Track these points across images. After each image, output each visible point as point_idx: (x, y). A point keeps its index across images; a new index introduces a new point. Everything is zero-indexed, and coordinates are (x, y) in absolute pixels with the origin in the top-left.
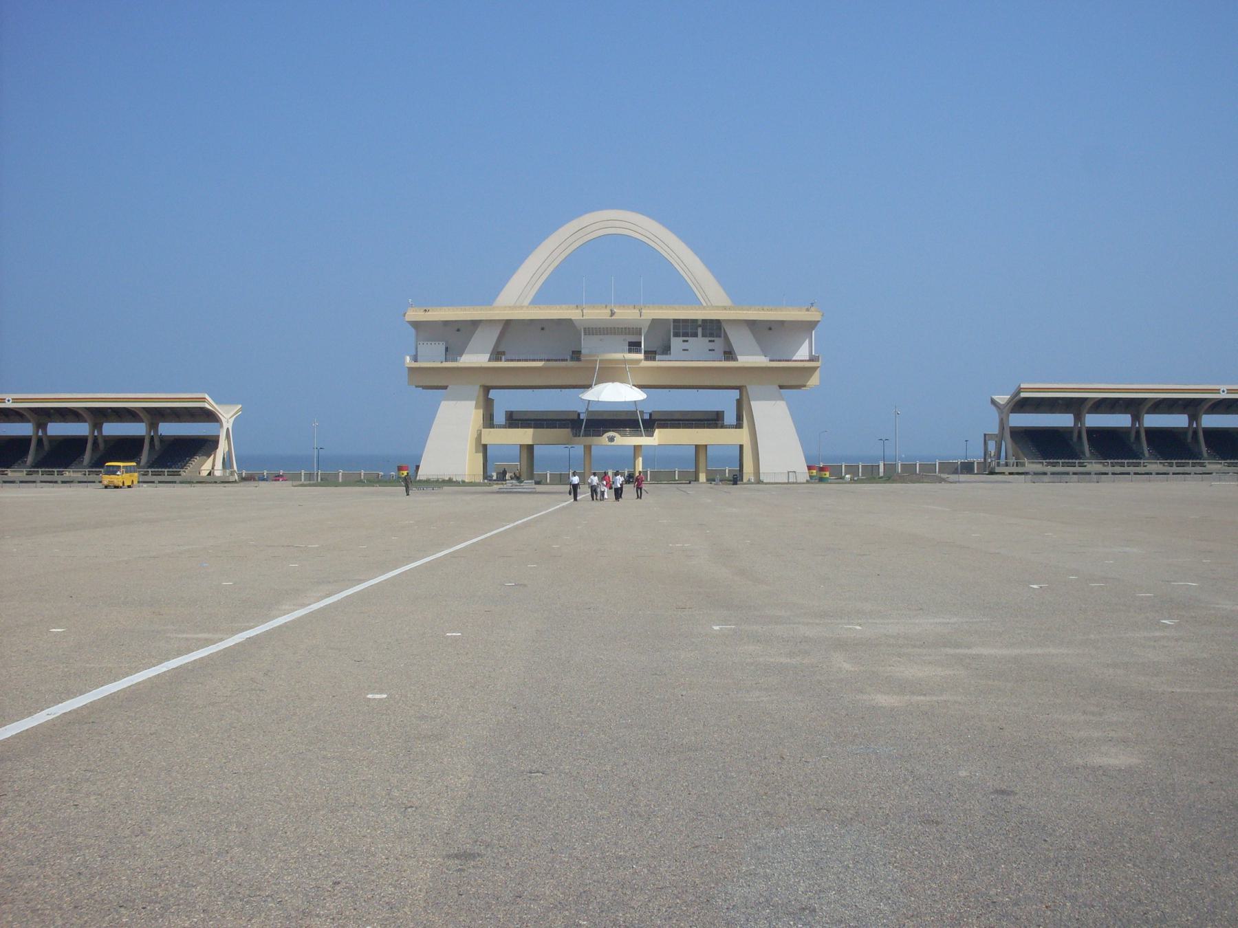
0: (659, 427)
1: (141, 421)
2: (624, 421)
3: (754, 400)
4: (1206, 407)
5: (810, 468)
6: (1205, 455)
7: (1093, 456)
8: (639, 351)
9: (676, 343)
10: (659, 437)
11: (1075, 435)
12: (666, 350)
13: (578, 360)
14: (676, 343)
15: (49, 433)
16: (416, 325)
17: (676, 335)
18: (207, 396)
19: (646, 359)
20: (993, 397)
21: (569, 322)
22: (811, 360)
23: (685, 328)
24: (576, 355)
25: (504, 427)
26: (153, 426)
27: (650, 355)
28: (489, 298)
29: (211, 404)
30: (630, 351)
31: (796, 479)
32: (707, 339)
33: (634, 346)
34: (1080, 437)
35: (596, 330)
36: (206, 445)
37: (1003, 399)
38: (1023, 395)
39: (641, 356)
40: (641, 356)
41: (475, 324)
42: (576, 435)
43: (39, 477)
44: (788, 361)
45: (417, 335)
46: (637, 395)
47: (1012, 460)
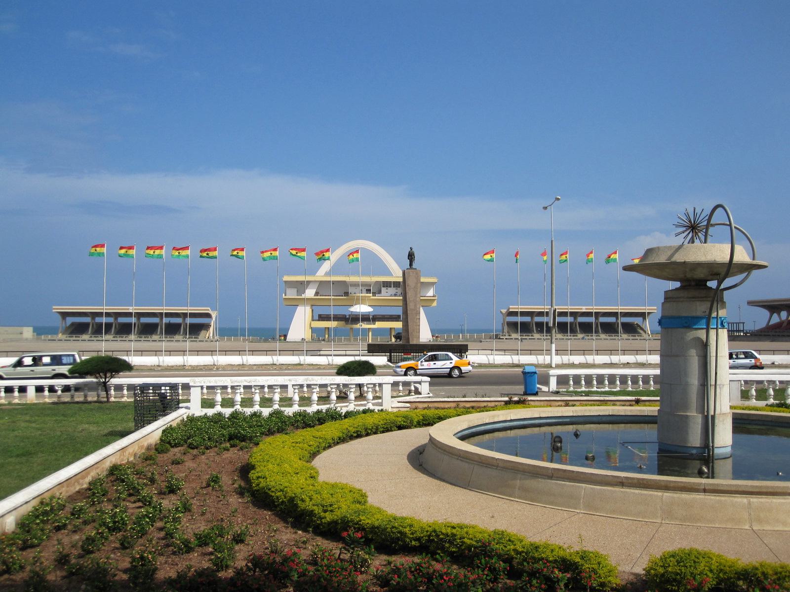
0: (378, 321)
1: (181, 317)
2: (366, 318)
3: (737, 244)
4: (579, 314)
5: (433, 336)
6: (600, 332)
7: (581, 333)
8: (370, 293)
9: (384, 290)
10: (379, 325)
11: (574, 324)
12: (380, 292)
13: (348, 296)
14: (384, 290)
15: (96, 321)
16: (286, 282)
17: (383, 287)
18: (209, 308)
19: (373, 296)
20: (502, 310)
21: (345, 282)
22: (433, 296)
23: (387, 284)
24: (346, 294)
25: (319, 320)
26: (116, 319)
27: (374, 294)
28: (314, 273)
29: (210, 312)
30: (367, 293)
31: (537, 358)
32: (395, 288)
33: (368, 291)
34: (576, 325)
35: (355, 285)
36: (206, 327)
37: (504, 311)
38: (510, 310)
39: (371, 295)
40: (371, 295)
41: (309, 282)
42: (347, 324)
43: (143, 339)
44: (425, 297)
45: (286, 285)
46: (370, 309)
47: (507, 334)
